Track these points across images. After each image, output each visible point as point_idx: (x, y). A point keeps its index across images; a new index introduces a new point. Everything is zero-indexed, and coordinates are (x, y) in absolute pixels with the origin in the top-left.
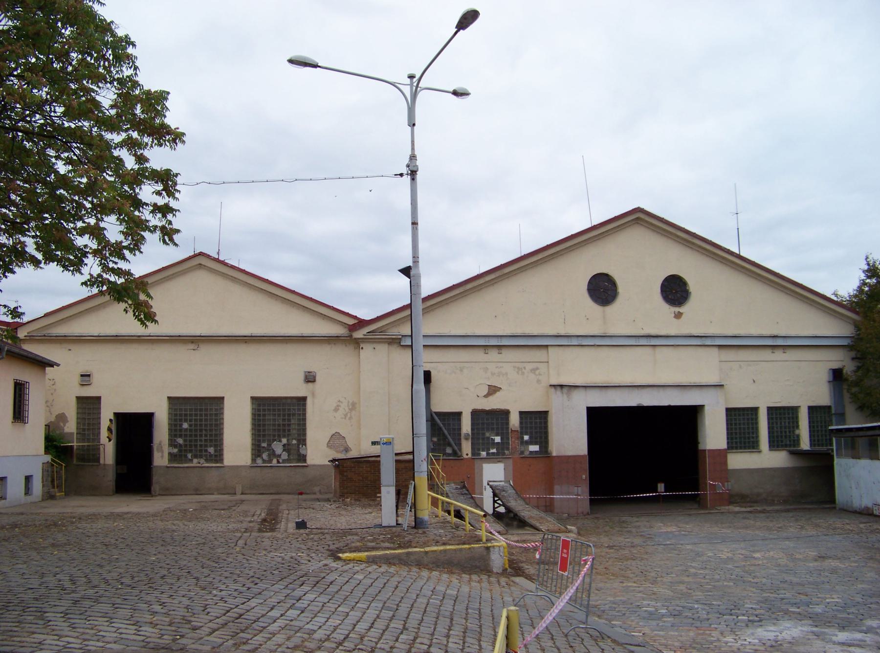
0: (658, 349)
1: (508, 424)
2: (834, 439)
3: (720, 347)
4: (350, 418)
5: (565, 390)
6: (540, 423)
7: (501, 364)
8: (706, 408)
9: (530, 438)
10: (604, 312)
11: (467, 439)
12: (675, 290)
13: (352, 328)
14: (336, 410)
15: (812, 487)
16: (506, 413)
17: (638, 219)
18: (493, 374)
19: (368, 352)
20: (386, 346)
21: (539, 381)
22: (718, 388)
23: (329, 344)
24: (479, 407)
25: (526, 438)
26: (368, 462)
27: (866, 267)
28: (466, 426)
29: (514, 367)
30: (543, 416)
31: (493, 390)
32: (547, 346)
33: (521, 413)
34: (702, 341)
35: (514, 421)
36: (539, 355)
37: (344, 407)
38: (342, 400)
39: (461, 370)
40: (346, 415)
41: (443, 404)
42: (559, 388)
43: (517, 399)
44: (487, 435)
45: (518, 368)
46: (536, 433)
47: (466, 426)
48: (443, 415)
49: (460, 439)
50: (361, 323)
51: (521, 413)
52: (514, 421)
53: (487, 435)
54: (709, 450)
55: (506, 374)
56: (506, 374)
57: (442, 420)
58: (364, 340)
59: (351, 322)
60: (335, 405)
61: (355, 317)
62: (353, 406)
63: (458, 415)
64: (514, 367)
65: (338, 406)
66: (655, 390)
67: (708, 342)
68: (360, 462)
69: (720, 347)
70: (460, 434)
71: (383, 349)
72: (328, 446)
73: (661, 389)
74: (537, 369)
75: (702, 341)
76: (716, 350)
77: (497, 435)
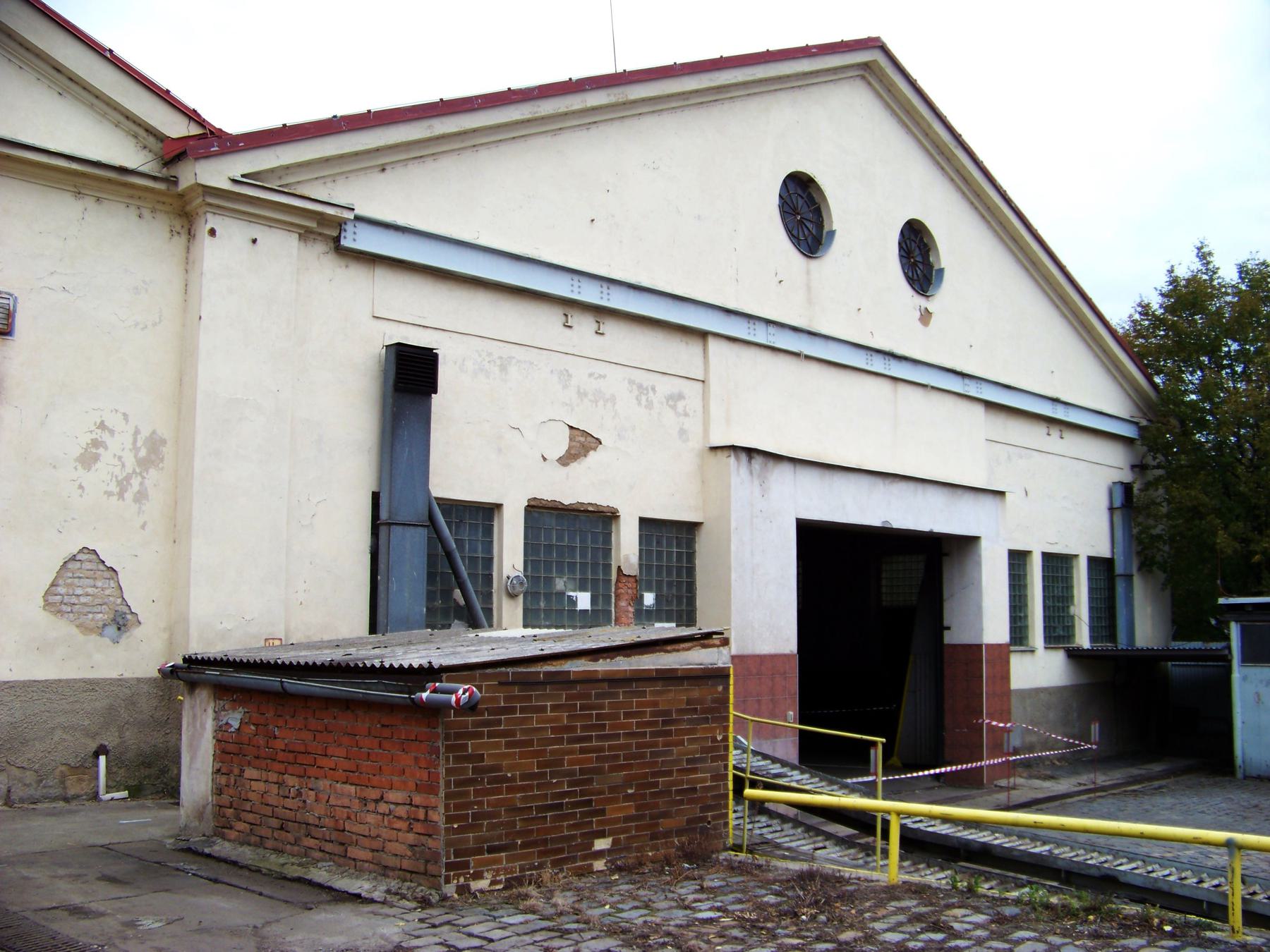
0: (904, 390)
1: (607, 552)
3: (990, 405)
4: (141, 496)
5: (758, 462)
6: (679, 555)
7: (600, 368)
8: (984, 544)
9: (657, 598)
10: (808, 273)
11: (512, 596)
12: (918, 254)
13: (175, 153)
14: (88, 459)
16: (606, 518)
17: (866, 66)
18: (582, 394)
19: (228, 248)
20: (292, 240)
21: (682, 432)
22: (989, 501)
23: (78, 194)
24: (547, 495)
25: (649, 599)
26: (563, 680)
27: (1166, 288)
28: (510, 554)
29: (631, 382)
30: (687, 531)
31: (582, 444)
32: (703, 335)
33: (643, 521)
34: (960, 385)
35: (627, 546)
36: (683, 354)
37: (119, 444)
38: (113, 421)
39: (503, 368)
40: (123, 484)
41: (455, 472)
42: (744, 457)
43: (636, 483)
44: (560, 584)
45: (640, 386)
46: (670, 584)
47: (510, 554)
48: (454, 508)
49: (487, 597)
50: (210, 141)
51: (643, 521)
52: (627, 546)
53: (560, 584)
54: (987, 645)
55: (613, 399)
56: (613, 399)
57: (455, 525)
58: (227, 201)
59: (177, 128)
60: (86, 439)
61: (192, 116)
62: (152, 452)
63: (608, 517)
64: (631, 382)
65: (96, 443)
66: (911, 485)
67: (972, 389)
68: (529, 683)
69: (990, 405)
70: (488, 579)
71: (281, 248)
72: (47, 605)
73: (920, 486)
74: (681, 396)
75: (960, 385)
76: (979, 410)
77: (583, 588)
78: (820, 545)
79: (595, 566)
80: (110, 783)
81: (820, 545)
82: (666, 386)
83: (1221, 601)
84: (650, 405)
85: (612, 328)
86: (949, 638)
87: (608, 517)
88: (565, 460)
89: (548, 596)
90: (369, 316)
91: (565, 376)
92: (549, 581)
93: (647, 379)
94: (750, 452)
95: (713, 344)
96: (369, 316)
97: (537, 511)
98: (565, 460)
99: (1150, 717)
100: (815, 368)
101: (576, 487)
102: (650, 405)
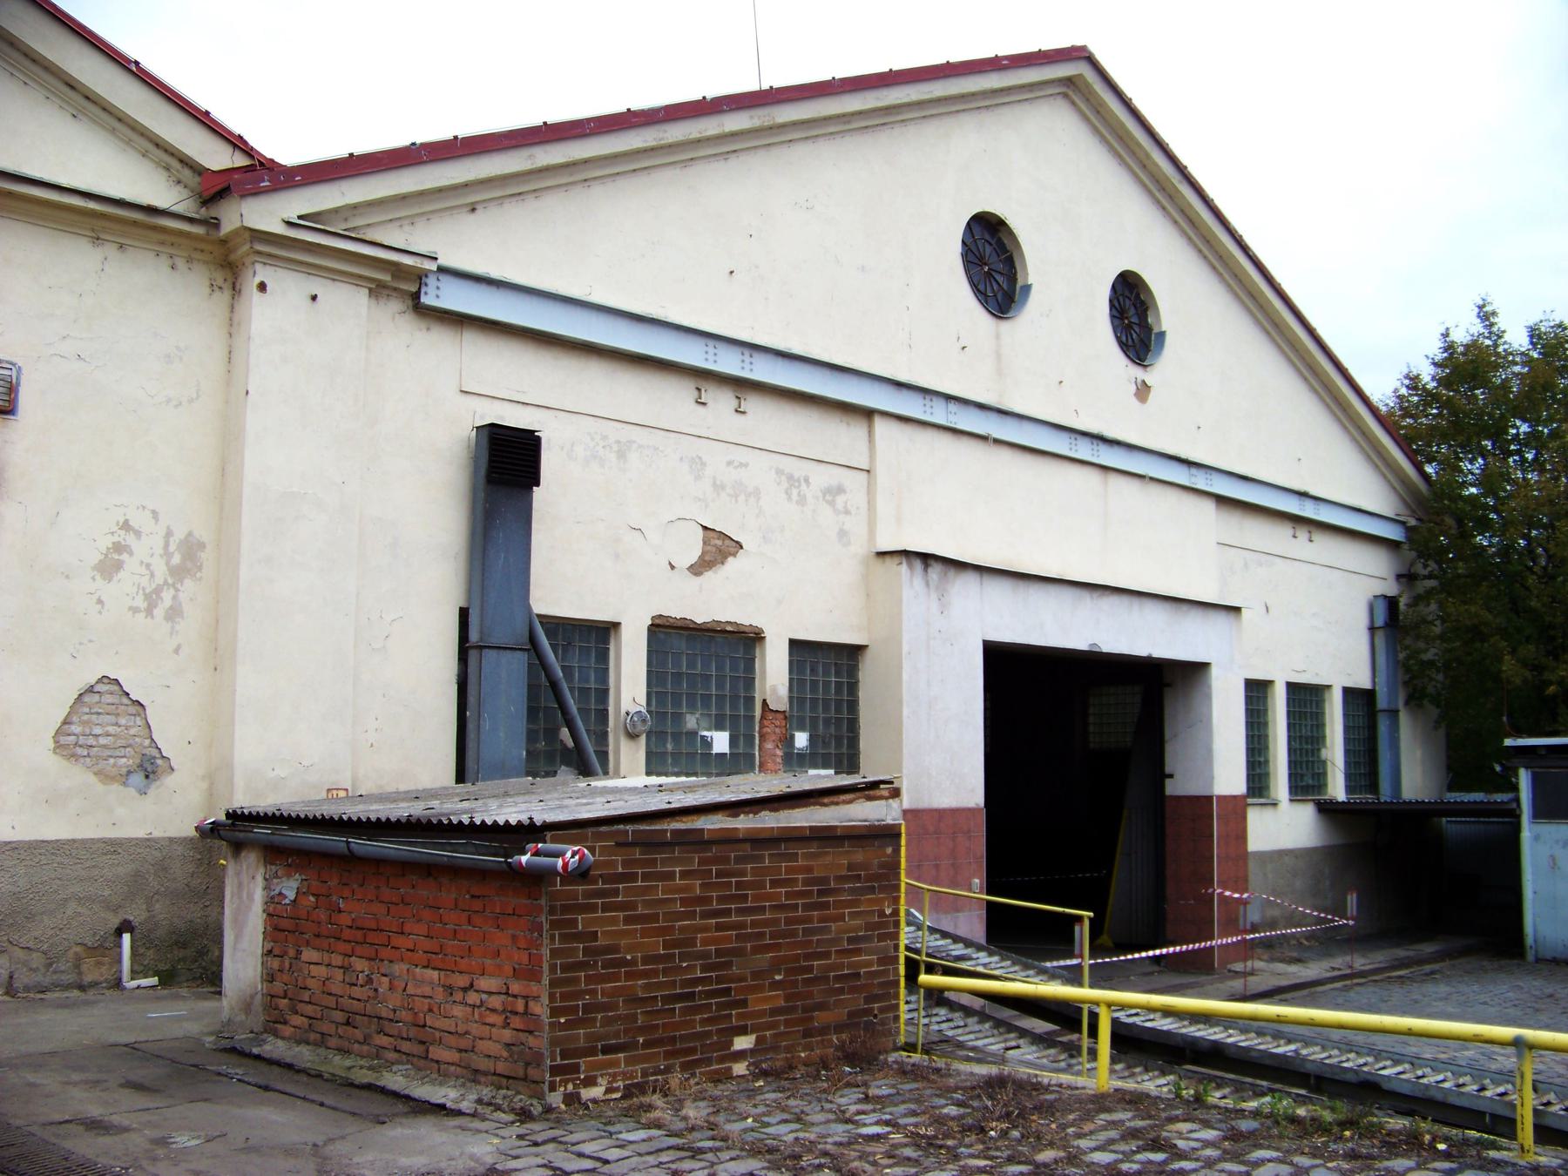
0: (1116, 481)
1: (750, 682)
2: (1508, 742)
3: (1222, 501)
4: (174, 613)
5: (936, 570)
6: (839, 685)
7: (741, 455)
8: (1215, 672)
9: (812, 739)
10: (998, 337)
11: (632, 736)
12: (1133, 314)
13: (216, 190)
14: (109, 567)
15: (1420, 886)
16: (749, 640)
17: (1069, 81)
18: (718, 487)
19: (281, 306)
20: (361, 297)
21: (842, 534)
22: (1220, 619)
23: (97, 240)
24: (676, 611)
25: (801, 740)
28: (630, 685)
29: (779, 472)
30: (848, 656)
31: (718, 549)
32: (868, 414)
33: (794, 644)
34: (1185, 475)
35: (774, 675)
36: (843, 438)
37: (147, 549)
38: (139, 520)
39: (621, 455)
40: (152, 598)
41: (561, 584)
42: (918, 564)
43: (785, 597)
44: (691, 722)
45: (790, 477)
46: (827, 722)
47: (630, 685)
48: (560, 628)
49: (602, 737)
50: (260, 174)
51: (794, 644)
52: (774, 675)
53: (691, 722)
54: (1219, 797)
55: (756, 493)
56: (756, 493)
57: (562, 649)
58: (281, 248)
59: (218, 158)
60: (106, 542)
61: (237, 143)
62: (188, 558)
63: (751, 639)
64: (779, 472)
65: (119, 548)
66: (1125, 599)
67: (1200, 481)
69: (1222, 501)
70: (603, 715)
71: (347, 306)
72: (59, 747)
73: (1136, 601)
74: (840, 490)
75: (1185, 475)
76: (1209, 506)
77: (719, 727)
78: (1012, 673)
79: (735, 699)
81: (1012, 673)
82: (822, 477)
84: (802, 501)
85: (756, 406)
86: (1172, 788)
87: (751, 639)
88: (698, 568)
89: (677, 736)
90: (456, 390)
91: (698, 464)
92: (678, 718)
93: (799, 469)
94: (926, 558)
95: (880, 425)
96: (456, 390)
97: (663, 632)
98: (698, 568)
100: (1006, 454)
101: (711, 601)
102: (802, 501)
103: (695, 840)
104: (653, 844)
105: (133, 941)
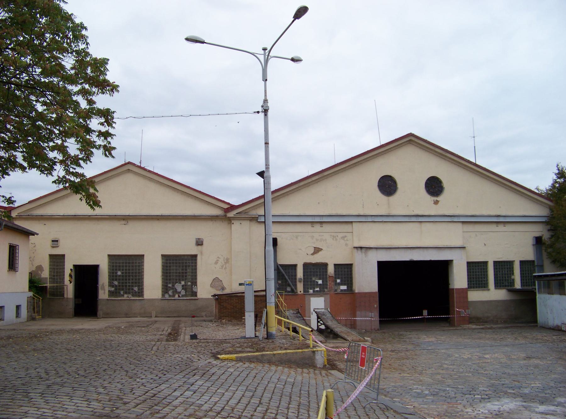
0: (423, 224)
1: (326, 272)
3: (463, 222)
4: (225, 268)
5: (363, 250)
6: (348, 271)
7: (322, 234)
8: (454, 262)
9: (341, 281)
10: (388, 200)
11: (300, 282)
12: (434, 186)
13: (227, 211)
14: (216, 263)
16: (325, 265)
17: (410, 140)
18: (317, 240)
19: (236, 226)
20: (248, 222)
21: (346, 245)
22: (462, 249)
23: (212, 220)
24: (308, 261)
25: (338, 281)
28: (300, 273)
29: (331, 236)
30: (349, 267)
31: (317, 250)
32: (352, 222)
33: (335, 265)
34: (451, 219)
35: (331, 270)
36: (347, 228)
37: (221, 261)
38: (220, 256)
39: (297, 238)
40: (222, 267)
41: (285, 259)
42: (359, 249)
43: (332, 256)
44: (313, 279)
45: (333, 236)
46: (345, 278)
47: (300, 273)
48: (285, 267)
49: (296, 282)
50: (232, 207)
51: (335, 265)
52: (331, 270)
53: (313, 279)
54: (456, 289)
55: (326, 240)
56: (326, 240)
57: (284, 270)
58: (234, 218)
59: (226, 206)
60: (215, 260)
61: (228, 204)
62: (227, 261)
64: (331, 236)
65: (217, 260)
66: (421, 250)
67: (456, 219)
69: (463, 222)
70: (296, 279)
71: (246, 224)
72: (211, 286)
73: (425, 250)
74: (346, 237)
75: (451, 219)
76: (460, 224)
77: (320, 279)
80: (264, 298)
83: (536, 282)
99: (522, 312)
103: (237, 296)
104: (232, 296)
105: (308, 330)
